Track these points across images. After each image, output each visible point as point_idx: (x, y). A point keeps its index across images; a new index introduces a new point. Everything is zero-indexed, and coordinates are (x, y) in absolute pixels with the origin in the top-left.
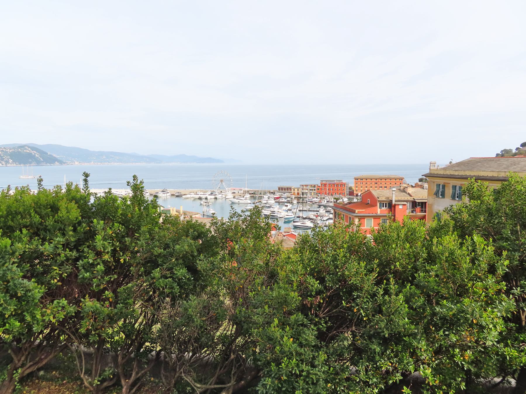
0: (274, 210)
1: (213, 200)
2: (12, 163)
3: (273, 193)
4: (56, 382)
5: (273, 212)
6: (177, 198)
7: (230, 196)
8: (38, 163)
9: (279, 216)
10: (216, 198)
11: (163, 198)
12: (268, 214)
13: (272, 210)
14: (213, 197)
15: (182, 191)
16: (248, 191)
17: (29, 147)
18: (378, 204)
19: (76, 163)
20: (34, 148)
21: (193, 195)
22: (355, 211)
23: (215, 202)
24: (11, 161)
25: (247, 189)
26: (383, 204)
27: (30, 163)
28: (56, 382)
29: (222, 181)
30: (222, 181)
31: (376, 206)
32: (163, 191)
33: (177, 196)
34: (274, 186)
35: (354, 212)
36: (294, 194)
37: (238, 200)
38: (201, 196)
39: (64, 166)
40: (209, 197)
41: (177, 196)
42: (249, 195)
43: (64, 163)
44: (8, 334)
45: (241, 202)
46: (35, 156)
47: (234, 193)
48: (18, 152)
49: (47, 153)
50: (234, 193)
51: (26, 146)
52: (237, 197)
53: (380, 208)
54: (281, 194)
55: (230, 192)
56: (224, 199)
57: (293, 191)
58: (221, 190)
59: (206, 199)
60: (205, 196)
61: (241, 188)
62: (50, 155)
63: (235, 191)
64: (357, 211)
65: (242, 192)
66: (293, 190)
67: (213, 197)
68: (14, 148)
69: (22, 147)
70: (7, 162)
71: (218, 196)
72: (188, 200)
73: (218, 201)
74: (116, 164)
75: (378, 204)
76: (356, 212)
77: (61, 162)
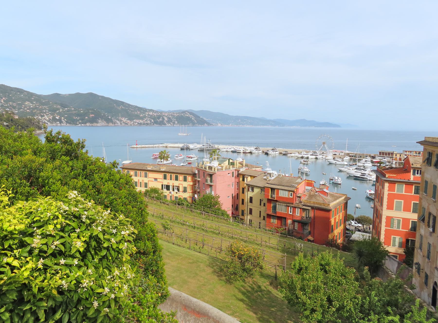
0: (365, 173)
1: (314, 160)
2: (177, 124)
3: (374, 157)
4: (42, 171)
5: (363, 174)
6: (284, 156)
7: (330, 157)
8: (194, 124)
9: (368, 178)
10: (317, 158)
11: (256, 154)
12: (359, 176)
13: (363, 172)
14: (314, 157)
15: (289, 150)
16: (349, 154)
17: (188, 112)
18: (412, 171)
19: (219, 125)
20: (191, 113)
21: (297, 155)
22: (386, 175)
23: (315, 162)
24: (176, 122)
25: (347, 152)
26: (418, 171)
27: (188, 124)
28: (42, 171)
29: (324, 143)
30: (324, 143)
31: (410, 172)
32: (273, 150)
33: (284, 155)
34: (375, 151)
35: (384, 176)
36: (396, 159)
37: (335, 161)
38: (304, 155)
39: (210, 127)
40: (310, 157)
41: (284, 155)
42: (349, 158)
43: (211, 125)
44: (363, 314)
45: (338, 163)
46: (192, 119)
47: (335, 155)
48: (181, 116)
49: (200, 117)
50: (335, 155)
51: (186, 111)
52: (336, 159)
53: (414, 174)
54: (381, 158)
55: (331, 154)
56: (324, 160)
57: (394, 156)
58: (323, 151)
59: (308, 158)
60: (307, 156)
61: (342, 151)
62: (202, 118)
63: (336, 153)
64: (387, 176)
65: (343, 154)
66: (395, 155)
67: (314, 157)
68: (179, 113)
69: (184, 112)
70: (174, 123)
71: (319, 157)
72: (133, 149)
73: (318, 161)
74: (248, 126)
75: (412, 171)
76: (387, 176)
77: (209, 124)
